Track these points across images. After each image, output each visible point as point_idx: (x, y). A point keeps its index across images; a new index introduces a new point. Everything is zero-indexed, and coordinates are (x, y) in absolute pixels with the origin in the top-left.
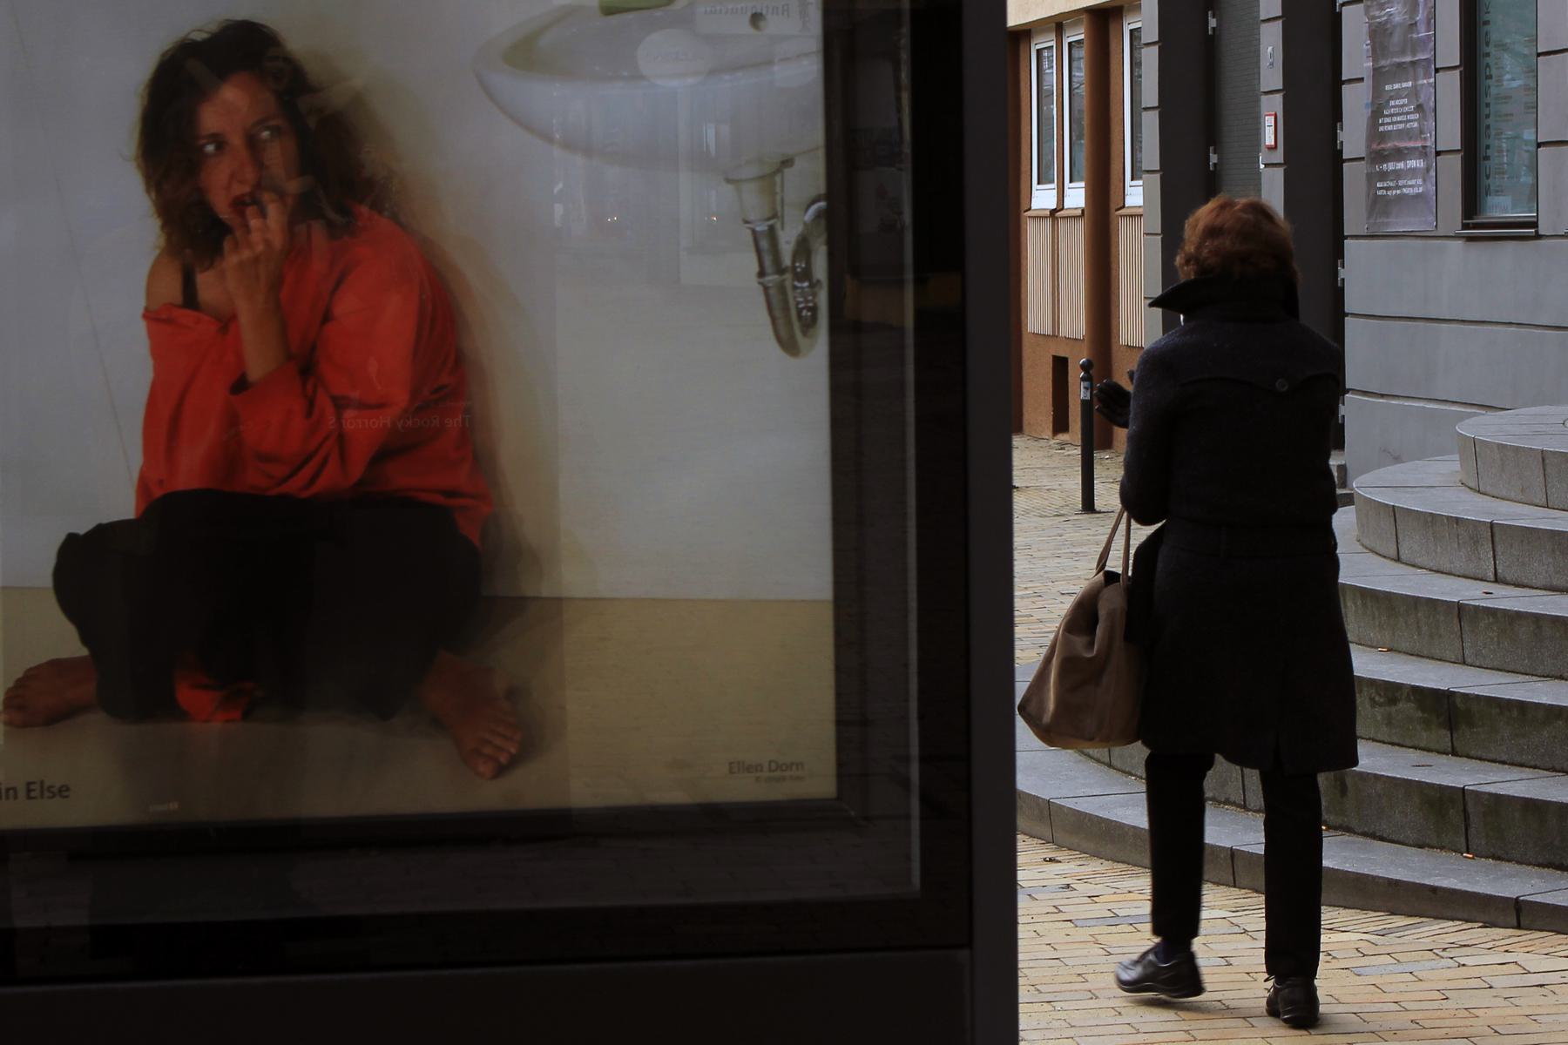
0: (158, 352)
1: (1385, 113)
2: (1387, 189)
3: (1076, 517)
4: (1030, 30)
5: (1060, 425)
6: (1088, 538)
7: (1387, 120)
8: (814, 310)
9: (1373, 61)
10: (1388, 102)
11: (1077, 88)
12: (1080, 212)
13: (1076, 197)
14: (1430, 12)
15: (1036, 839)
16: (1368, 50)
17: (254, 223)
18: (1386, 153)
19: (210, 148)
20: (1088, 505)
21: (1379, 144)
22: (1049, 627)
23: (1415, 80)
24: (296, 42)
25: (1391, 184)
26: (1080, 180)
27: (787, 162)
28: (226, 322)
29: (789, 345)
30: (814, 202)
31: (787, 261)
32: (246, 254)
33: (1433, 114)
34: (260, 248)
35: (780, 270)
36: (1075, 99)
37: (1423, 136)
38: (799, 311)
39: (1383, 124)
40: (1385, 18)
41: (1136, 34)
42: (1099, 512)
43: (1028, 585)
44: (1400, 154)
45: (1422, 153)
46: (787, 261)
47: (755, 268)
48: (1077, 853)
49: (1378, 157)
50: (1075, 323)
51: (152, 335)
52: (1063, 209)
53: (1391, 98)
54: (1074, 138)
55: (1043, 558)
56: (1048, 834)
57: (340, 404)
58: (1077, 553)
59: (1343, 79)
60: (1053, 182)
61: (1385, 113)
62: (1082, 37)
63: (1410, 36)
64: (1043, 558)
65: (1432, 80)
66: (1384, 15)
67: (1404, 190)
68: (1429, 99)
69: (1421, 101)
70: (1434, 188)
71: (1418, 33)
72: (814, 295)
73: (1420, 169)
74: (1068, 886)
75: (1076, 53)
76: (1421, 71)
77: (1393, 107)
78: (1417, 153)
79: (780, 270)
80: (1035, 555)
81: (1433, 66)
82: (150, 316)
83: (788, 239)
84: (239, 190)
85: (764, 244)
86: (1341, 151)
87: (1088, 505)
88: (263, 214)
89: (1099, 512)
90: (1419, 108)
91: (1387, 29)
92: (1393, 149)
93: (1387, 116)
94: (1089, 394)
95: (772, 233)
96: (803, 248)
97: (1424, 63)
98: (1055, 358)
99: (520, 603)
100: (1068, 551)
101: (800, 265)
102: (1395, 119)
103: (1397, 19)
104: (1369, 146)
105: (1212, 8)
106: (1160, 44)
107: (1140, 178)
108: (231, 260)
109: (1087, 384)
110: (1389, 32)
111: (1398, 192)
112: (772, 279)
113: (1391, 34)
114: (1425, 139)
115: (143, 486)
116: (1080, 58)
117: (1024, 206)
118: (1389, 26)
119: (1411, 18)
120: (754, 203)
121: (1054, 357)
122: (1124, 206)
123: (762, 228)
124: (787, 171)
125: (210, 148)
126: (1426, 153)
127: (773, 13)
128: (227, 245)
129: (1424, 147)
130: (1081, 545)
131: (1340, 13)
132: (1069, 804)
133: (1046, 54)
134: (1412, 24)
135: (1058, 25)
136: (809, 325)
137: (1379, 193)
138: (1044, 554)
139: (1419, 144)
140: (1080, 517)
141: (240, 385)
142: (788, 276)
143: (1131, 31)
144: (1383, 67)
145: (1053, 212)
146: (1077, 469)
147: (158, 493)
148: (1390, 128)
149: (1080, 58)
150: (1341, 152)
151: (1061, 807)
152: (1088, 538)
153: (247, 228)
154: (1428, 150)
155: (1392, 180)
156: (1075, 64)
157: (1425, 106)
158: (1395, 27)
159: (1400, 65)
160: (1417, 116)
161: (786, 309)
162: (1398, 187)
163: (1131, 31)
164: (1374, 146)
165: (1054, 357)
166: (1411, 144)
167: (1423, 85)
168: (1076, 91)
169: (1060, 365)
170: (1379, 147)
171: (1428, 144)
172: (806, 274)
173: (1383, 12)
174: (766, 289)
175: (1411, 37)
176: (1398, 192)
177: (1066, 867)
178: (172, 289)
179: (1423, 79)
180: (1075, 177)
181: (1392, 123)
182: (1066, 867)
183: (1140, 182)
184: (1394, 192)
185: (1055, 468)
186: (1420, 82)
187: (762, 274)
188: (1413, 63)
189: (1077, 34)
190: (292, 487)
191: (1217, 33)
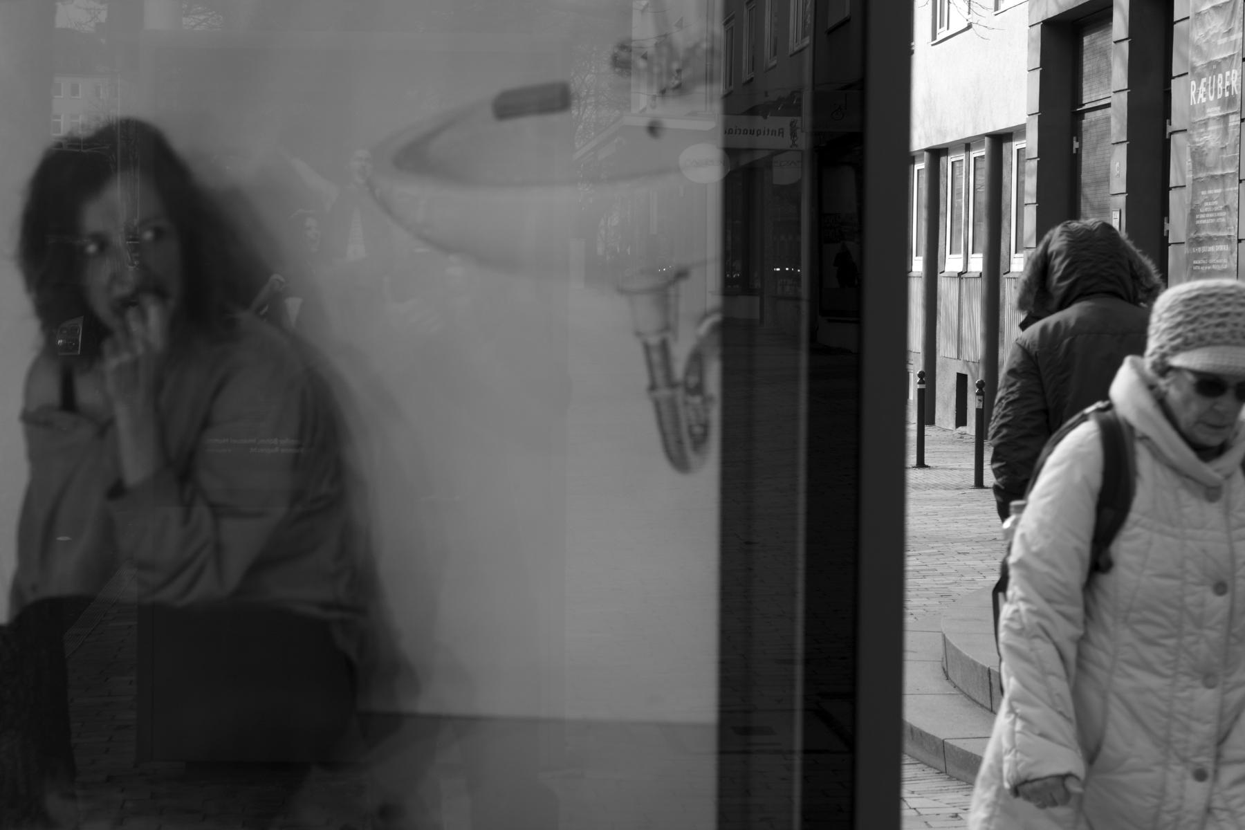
0: (36, 456)
1: (1201, 211)
2: (1200, 265)
3: (970, 491)
4: (947, 148)
5: (961, 420)
6: (979, 508)
7: (1202, 216)
8: (706, 426)
9: (1193, 173)
10: (1203, 203)
11: (979, 188)
12: (978, 275)
13: (977, 264)
14: (1236, 140)
15: (933, 769)
16: (1189, 166)
17: (135, 327)
18: (1201, 240)
19: (92, 248)
20: (979, 483)
21: (1195, 233)
22: (948, 580)
23: (1224, 188)
24: (180, 143)
25: (1204, 262)
26: (979, 252)
27: (682, 274)
28: (105, 427)
29: (679, 462)
30: (706, 315)
31: (679, 370)
32: (126, 357)
33: (1237, 213)
34: (140, 350)
35: (672, 385)
36: (977, 195)
37: (1228, 228)
38: (690, 427)
39: (1199, 219)
40: (1203, 143)
41: (1021, 152)
42: (987, 488)
43: (935, 545)
44: (1211, 240)
45: (1228, 240)
46: (679, 370)
47: (645, 381)
48: (965, 783)
49: (1198, 242)
50: (975, 348)
51: (30, 438)
52: (966, 272)
53: (1206, 200)
54: (975, 221)
55: (945, 523)
56: (942, 766)
57: (218, 511)
58: (970, 520)
59: (1170, 186)
60: (960, 253)
61: (1201, 211)
62: (984, 153)
63: (1220, 156)
64: (945, 523)
65: (1237, 188)
66: (1202, 142)
67: (1214, 267)
68: (1234, 201)
69: (1228, 203)
70: (1236, 265)
71: (1227, 154)
72: (707, 411)
73: (1226, 251)
74: (956, 816)
75: (979, 165)
76: (1228, 181)
77: (1207, 207)
78: (1224, 240)
79: (672, 385)
80: (940, 520)
81: (1238, 178)
82: (29, 418)
83: (681, 352)
84: (121, 291)
85: (656, 357)
86: (1167, 237)
87: (979, 483)
88: (143, 317)
89: (987, 488)
90: (1226, 208)
91: (1203, 151)
92: (1206, 237)
93: (1202, 213)
94: (982, 405)
95: (664, 347)
96: (697, 358)
97: (1231, 176)
98: (959, 375)
99: (395, 721)
100: (964, 518)
101: (693, 380)
102: (1208, 215)
103: (1212, 144)
104: (1187, 235)
105: (1076, 135)
106: (1128, 143)
107: (1022, 252)
108: (112, 363)
109: (981, 397)
110: (1205, 153)
111: (1209, 268)
112: (664, 393)
113: (1207, 154)
114: (1230, 230)
115: (17, 592)
116: (981, 168)
117: (940, 270)
118: (1205, 149)
119: (1222, 143)
120: (648, 316)
121: (958, 374)
122: (1009, 272)
123: (654, 340)
124: (683, 285)
125: (92, 248)
126: (1230, 240)
127: (772, 134)
128: (107, 346)
129: (1229, 236)
130: (973, 513)
131: (1169, 140)
132: (959, 744)
133: (957, 165)
134: (1222, 148)
135: (967, 145)
136: (700, 442)
137: (1195, 268)
138: (946, 519)
139: (1225, 234)
140: (973, 491)
141: (117, 490)
142: (680, 393)
143: (1018, 150)
144: (1200, 178)
145: (960, 274)
146: (971, 453)
147: (31, 598)
148: (1204, 222)
149: (981, 168)
150: (1167, 238)
151: (952, 747)
152: (979, 508)
153: (126, 329)
154: (1232, 238)
155: (1205, 259)
156: (978, 172)
157: (1231, 206)
158: (1209, 149)
159: (1212, 177)
160: (1224, 214)
161: (676, 423)
162: (1209, 264)
163: (1018, 150)
164: (1192, 235)
165: (958, 374)
166: (1220, 234)
167: (1230, 191)
168: (978, 190)
169: (962, 379)
170: (1195, 236)
171: (1232, 234)
172: (699, 389)
173: (1201, 139)
174: (657, 404)
175: (1222, 158)
176: (1209, 268)
177: (956, 796)
178: (50, 391)
179: (1230, 187)
180: (976, 249)
181: (1206, 218)
182: (956, 796)
183: (1022, 255)
184: (1206, 268)
185: (955, 452)
186: (1228, 189)
187: (653, 387)
188: (1223, 176)
189: (981, 152)
190: (168, 595)
191: (1079, 152)
